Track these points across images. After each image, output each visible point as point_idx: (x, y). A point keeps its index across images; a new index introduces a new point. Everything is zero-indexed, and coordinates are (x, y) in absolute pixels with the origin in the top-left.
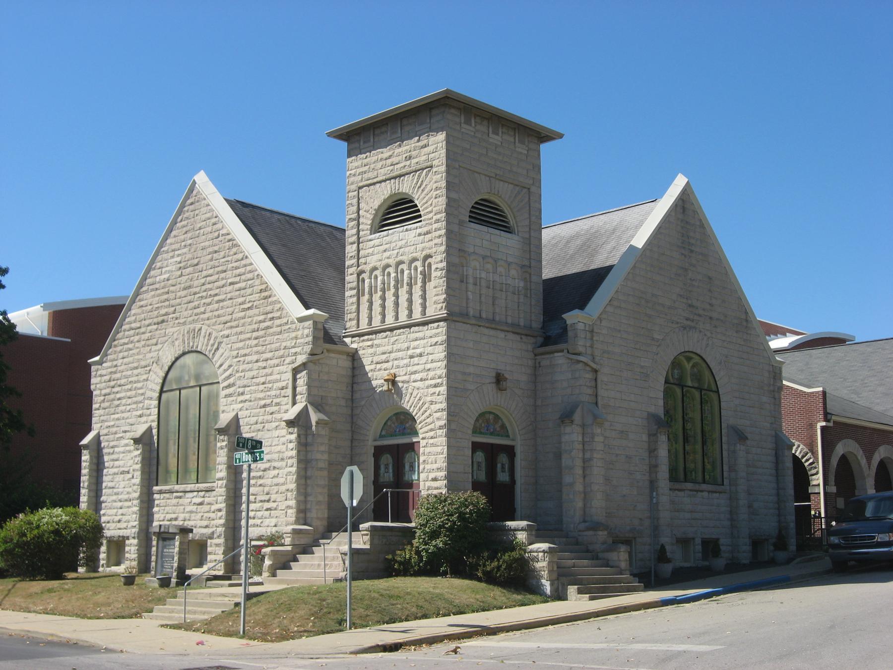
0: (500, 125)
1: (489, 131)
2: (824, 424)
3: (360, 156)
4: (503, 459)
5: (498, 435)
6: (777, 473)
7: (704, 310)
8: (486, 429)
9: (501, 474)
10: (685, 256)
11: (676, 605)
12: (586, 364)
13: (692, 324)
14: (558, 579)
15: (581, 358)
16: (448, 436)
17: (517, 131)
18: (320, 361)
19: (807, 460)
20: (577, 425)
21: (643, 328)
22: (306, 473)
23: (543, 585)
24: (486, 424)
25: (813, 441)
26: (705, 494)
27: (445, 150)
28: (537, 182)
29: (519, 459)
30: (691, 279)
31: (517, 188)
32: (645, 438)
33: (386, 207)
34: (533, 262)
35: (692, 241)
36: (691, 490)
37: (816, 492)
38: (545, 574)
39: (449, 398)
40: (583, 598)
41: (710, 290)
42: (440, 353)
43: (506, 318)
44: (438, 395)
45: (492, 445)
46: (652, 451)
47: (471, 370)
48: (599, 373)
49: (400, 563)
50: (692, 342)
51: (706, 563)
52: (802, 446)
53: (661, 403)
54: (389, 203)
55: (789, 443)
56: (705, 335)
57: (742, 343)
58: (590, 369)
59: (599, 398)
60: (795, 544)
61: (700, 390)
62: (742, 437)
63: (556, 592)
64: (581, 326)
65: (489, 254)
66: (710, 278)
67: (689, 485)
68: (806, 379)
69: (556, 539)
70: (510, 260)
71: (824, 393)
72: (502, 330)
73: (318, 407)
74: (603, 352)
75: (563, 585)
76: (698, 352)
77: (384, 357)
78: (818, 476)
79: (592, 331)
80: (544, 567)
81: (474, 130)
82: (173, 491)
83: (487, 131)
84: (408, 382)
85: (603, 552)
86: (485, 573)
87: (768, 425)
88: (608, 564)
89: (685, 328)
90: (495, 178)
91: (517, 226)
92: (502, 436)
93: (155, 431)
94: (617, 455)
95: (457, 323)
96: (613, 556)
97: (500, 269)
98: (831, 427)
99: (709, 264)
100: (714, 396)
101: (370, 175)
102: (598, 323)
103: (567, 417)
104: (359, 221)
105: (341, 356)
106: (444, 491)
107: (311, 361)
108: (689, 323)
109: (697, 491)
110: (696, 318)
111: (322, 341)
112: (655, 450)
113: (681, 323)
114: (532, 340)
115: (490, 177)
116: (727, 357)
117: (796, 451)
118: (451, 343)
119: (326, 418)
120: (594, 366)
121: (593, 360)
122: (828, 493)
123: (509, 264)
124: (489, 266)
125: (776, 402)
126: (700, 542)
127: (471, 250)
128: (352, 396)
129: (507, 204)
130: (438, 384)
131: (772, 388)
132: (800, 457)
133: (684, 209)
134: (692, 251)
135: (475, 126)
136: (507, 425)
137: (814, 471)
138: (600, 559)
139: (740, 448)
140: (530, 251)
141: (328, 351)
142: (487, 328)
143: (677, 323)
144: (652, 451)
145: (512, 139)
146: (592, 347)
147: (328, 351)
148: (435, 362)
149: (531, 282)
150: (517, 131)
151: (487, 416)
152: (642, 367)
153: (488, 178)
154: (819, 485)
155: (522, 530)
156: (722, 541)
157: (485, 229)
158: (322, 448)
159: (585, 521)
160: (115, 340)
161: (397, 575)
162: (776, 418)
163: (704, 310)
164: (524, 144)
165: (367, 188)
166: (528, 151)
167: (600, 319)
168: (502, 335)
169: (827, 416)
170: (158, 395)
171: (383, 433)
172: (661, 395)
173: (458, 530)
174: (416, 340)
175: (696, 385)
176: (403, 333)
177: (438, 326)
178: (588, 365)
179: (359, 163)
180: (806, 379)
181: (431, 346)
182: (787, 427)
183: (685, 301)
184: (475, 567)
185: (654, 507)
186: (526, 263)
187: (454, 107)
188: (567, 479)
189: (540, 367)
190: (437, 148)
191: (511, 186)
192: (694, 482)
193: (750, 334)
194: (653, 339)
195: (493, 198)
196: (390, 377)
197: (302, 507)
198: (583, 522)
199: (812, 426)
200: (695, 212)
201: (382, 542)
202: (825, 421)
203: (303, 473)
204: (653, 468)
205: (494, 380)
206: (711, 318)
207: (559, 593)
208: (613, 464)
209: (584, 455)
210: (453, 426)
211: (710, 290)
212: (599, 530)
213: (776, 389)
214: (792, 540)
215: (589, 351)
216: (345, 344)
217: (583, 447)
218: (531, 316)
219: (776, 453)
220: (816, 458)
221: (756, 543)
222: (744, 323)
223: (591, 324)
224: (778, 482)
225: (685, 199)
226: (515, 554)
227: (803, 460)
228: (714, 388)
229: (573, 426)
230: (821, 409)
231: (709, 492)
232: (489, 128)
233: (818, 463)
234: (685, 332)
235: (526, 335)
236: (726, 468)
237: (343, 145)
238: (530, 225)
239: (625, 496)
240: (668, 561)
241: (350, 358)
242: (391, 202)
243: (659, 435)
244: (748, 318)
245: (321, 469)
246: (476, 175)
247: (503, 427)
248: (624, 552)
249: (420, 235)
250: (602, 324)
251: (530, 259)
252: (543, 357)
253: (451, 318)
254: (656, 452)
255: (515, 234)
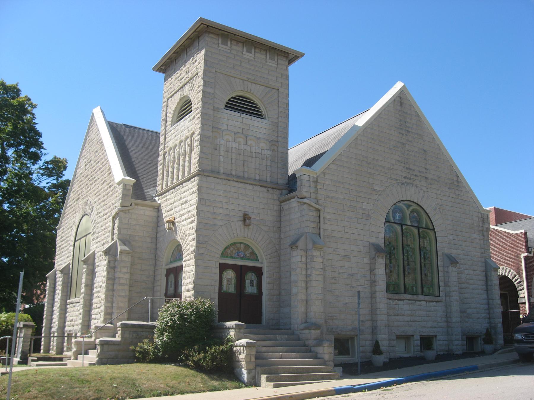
0: (253, 48)
1: (243, 50)
2: (526, 254)
3: (169, 79)
4: (251, 277)
5: (248, 259)
6: (487, 288)
7: (420, 172)
8: (236, 254)
9: (250, 287)
10: (403, 134)
11: (384, 388)
12: (310, 205)
13: (411, 181)
14: (255, 369)
15: (305, 201)
16: (196, 258)
17: (268, 52)
18: (131, 211)
19: (516, 280)
20: (301, 250)
21: (365, 182)
22: (113, 287)
23: (243, 374)
24: (237, 251)
25: (519, 267)
26: (423, 303)
27: (204, 61)
28: (286, 87)
29: (265, 277)
30: (408, 150)
31: (268, 89)
32: (366, 260)
33: (179, 108)
34: (280, 138)
35: (408, 125)
36: (409, 300)
37: (523, 302)
38: (243, 364)
39: (198, 231)
40: (270, 385)
41: (425, 159)
42: (194, 198)
43: (255, 176)
44: (192, 229)
45: (241, 266)
46: (372, 270)
47: (221, 211)
48: (321, 212)
49: (140, 352)
50: (411, 194)
51: (422, 354)
52: (512, 271)
53: (382, 236)
54: (181, 105)
55: (495, 267)
56: (421, 189)
57: (454, 196)
58: (314, 209)
59: (321, 230)
60: (503, 339)
61: (418, 228)
62: (453, 261)
63: (253, 379)
64: (305, 178)
65: (240, 131)
66: (425, 151)
67: (408, 296)
68: (531, 235)
69: (277, 336)
70: (260, 136)
71: (526, 234)
72: (250, 184)
73: (124, 242)
74: (327, 197)
75: (258, 373)
76: (415, 201)
77: (170, 207)
78: (524, 291)
79: (316, 182)
80: (243, 358)
81: (230, 49)
82: (73, 302)
83: (242, 51)
84: (180, 222)
85: (314, 346)
86: (194, 362)
87: (479, 254)
88: (317, 356)
89: (403, 184)
90: (248, 81)
91: (268, 114)
92: (252, 260)
93: (71, 266)
94: (339, 273)
95: (208, 178)
96: (320, 349)
97: (249, 142)
98: (531, 257)
99: (424, 141)
100: (431, 233)
101: (172, 90)
102: (322, 176)
103: (293, 245)
104: (166, 121)
105: (148, 208)
106: (192, 298)
107: (122, 211)
108: (407, 180)
109: (416, 300)
110: (413, 177)
111: (130, 197)
112: (374, 269)
113: (399, 180)
114: (278, 192)
115: (243, 80)
116: (441, 206)
117: (508, 274)
118: (200, 191)
119: (128, 249)
120: (317, 207)
121: (317, 203)
122: (532, 302)
123: (258, 139)
124: (241, 140)
125: (486, 239)
126: (419, 339)
127: (225, 127)
128: (157, 235)
129: (259, 99)
130: (192, 220)
131: (481, 228)
132: (511, 278)
133: (401, 104)
134: (409, 132)
135: (231, 46)
136: (257, 252)
137: (521, 288)
138: (313, 352)
139: (453, 271)
140: (278, 131)
141: (136, 204)
142: (236, 182)
143: (396, 180)
144: (372, 270)
145: (264, 57)
146: (316, 193)
147: (136, 204)
148: (178, 201)
149: (278, 152)
150: (268, 52)
151: (238, 245)
152: (364, 209)
153: (242, 81)
154: (524, 297)
155: (232, 328)
156: (439, 337)
157: (238, 114)
158: (125, 270)
159: (306, 322)
160: (65, 214)
161: (137, 362)
162: (485, 249)
163: (420, 172)
164: (274, 60)
165: (171, 98)
166: (277, 65)
167: (324, 173)
168: (251, 187)
169: (528, 250)
170: (73, 243)
171: (172, 260)
172: (382, 230)
173: (179, 328)
174: (185, 192)
175: (416, 225)
176: (179, 188)
177: (194, 180)
178: (311, 206)
179: (168, 84)
180: (531, 235)
181: (191, 195)
182: (495, 257)
183: (403, 165)
184: (187, 357)
185: (373, 311)
186: (274, 138)
187: (212, 33)
188: (294, 290)
189: (283, 210)
190: (200, 61)
191: (262, 88)
192: (412, 293)
193: (461, 191)
194: (374, 190)
195: (247, 95)
196: (172, 219)
197: (109, 311)
198: (305, 323)
199: (518, 257)
200: (411, 106)
201: (133, 336)
202: (526, 252)
203: (111, 287)
204: (373, 283)
205: (242, 219)
206: (426, 178)
207: (255, 380)
208: (335, 279)
209: (307, 272)
210: (201, 251)
211: (425, 159)
212: (312, 329)
213: (485, 229)
214: (500, 336)
215: (313, 196)
216: (155, 201)
217: (306, 266)
218: (278, 175)
219: (486, 274)
220: (522, 279)
221: (470, 339)
222: (456, 183)
223: (315, 176)
224: (488, 294)
225: (402, 97)
226: (224, 347)
227: (513, 281)
228: (431, 227)
229: (298, 250)
230: (524, 244)
231: (426, 301)
232: (243, 48)
233: (523, 282)
234: (403, 186)
235: (273, 188)
236: (441, 284)
237: (163, 75)
238: (278, 114)
239: (346, 303)
240: (381, 353)
241: (156, 210)
242: (181, 104)
243: (377, 258)
244: (459, 180)
245: (123, 285)
246: (231, 78)
247: (253, 253)
248: (327, 346)
249: (190, 120)
250: (325, 177)
251: (278, 136)
252: (285, 203)
253: (202, 173)
254: (374, 272)
255: (266, 119)
